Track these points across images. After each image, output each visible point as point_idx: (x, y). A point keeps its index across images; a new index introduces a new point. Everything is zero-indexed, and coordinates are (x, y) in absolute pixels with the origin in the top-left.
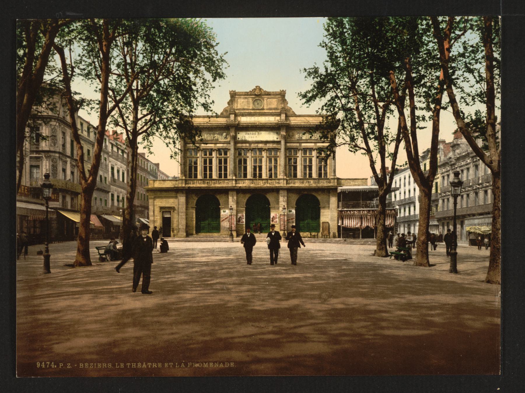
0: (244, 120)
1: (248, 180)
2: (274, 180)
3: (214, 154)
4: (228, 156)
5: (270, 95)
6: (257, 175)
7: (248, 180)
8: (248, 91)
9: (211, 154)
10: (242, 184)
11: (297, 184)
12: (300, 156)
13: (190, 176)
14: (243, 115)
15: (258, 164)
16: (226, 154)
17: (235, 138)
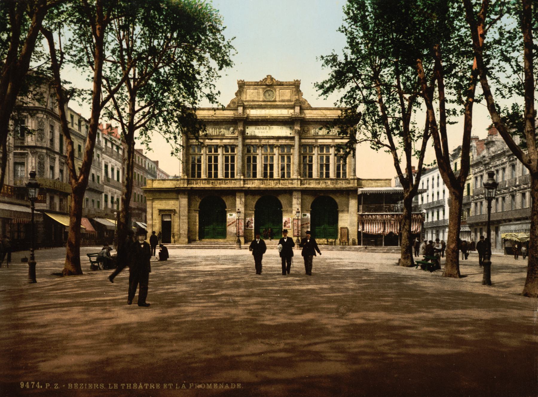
0: (254, 113)
1: (257, 180)
2: (287, 180)
3: (220, 151)
4: (236, 153)
5: (283, 85)
6: (268, 175)
7: (257, 180)
8: (258, 81)
9: (216, 151)
10: (250, 185)
11: (313, 185)
12: (316, 154)
13: (193, 176)
14: (252, 107)
15: (269, 163)
16: (233, 151)
17: (243, 133)
